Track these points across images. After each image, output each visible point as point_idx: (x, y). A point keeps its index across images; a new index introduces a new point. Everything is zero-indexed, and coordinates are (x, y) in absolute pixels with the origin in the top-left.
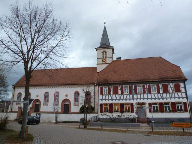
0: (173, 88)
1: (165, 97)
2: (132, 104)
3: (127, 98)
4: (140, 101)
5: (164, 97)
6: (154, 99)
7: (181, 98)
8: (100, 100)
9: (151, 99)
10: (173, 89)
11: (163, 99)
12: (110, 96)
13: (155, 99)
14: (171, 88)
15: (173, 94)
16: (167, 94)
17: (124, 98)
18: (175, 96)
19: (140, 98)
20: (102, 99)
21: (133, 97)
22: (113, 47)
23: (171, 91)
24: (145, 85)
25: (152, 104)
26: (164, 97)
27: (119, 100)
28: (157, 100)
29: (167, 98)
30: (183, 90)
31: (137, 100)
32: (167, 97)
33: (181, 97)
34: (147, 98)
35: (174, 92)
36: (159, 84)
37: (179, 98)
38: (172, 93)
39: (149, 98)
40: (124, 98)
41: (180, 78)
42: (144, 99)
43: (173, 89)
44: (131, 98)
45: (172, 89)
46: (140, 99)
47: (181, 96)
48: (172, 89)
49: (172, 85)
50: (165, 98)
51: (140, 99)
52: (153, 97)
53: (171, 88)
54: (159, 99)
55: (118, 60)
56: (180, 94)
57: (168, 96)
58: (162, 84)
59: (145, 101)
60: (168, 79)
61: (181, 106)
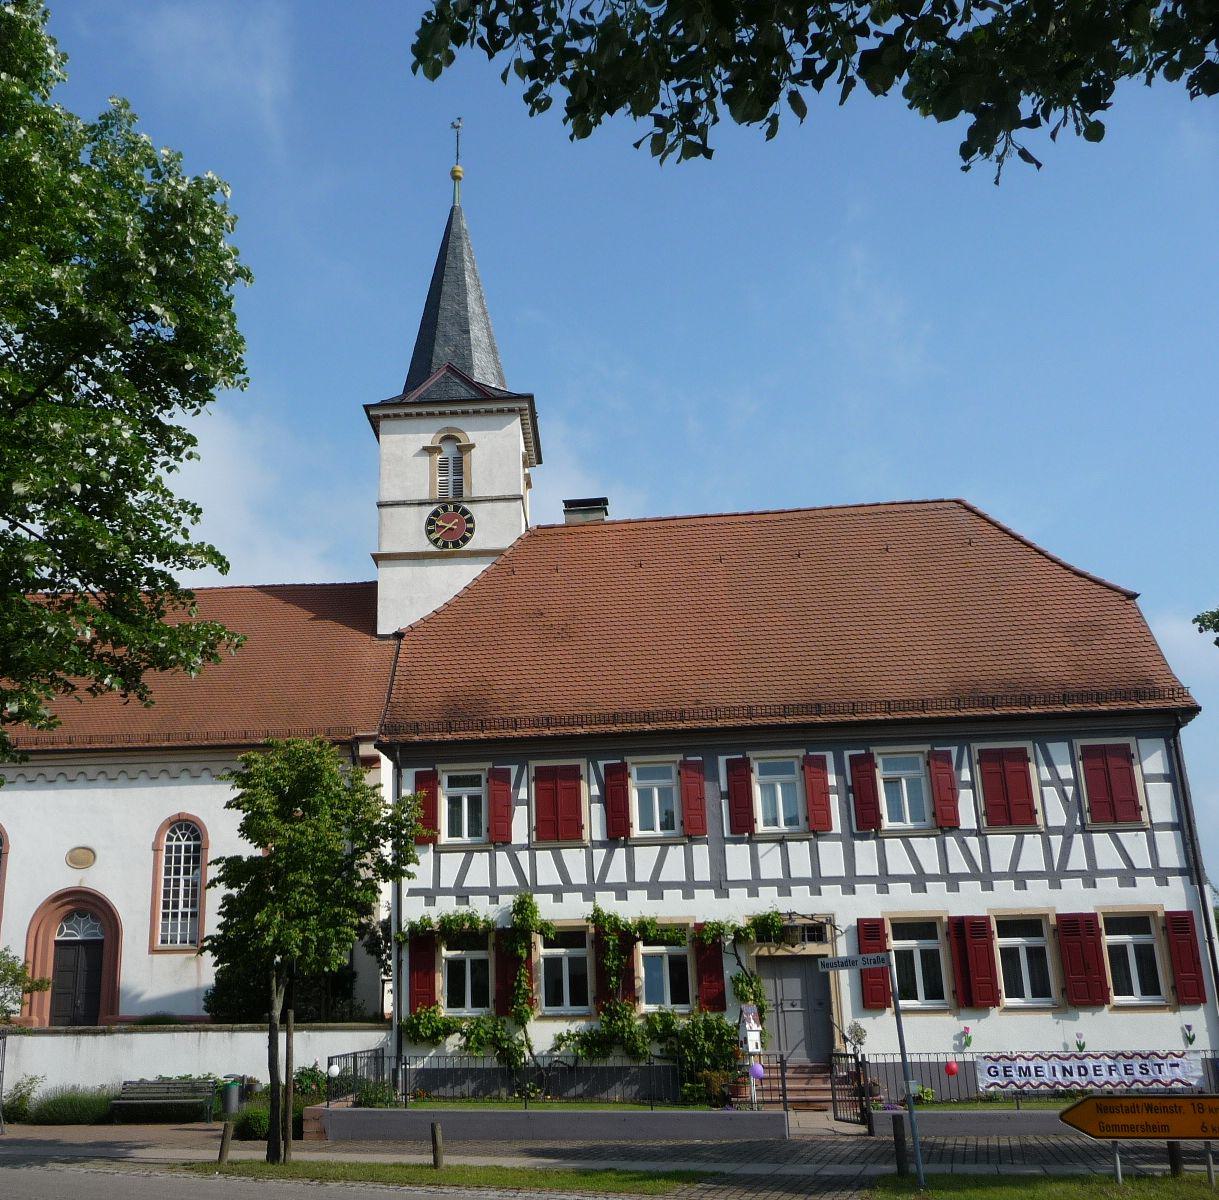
4: (784, 905)
5: (1000, 862)
11: (988, 886)
15: (1078, 839)
17: (639, 878)
19: (840, 871)
21: (719, 863)
22: (530, 398)
23: (1053, 809)
24: (830, 756)
25: (888, 929)
29: (1020, 879)
30: (1158, 802)
34: (683, 878)
36: (954, 750)
39: (801, 882)
40: (639, 878)
41: (1139, 695)
44: (703, 872)
46: (785, 885)
47: (1142, 860)
50: (1001, 876)
51: (785, 885)
54: (953, 881)
55: (579, 518)
56: (1135, 843)
57: (1033, 855)
58: (976, 747)
60: (1027, 701)
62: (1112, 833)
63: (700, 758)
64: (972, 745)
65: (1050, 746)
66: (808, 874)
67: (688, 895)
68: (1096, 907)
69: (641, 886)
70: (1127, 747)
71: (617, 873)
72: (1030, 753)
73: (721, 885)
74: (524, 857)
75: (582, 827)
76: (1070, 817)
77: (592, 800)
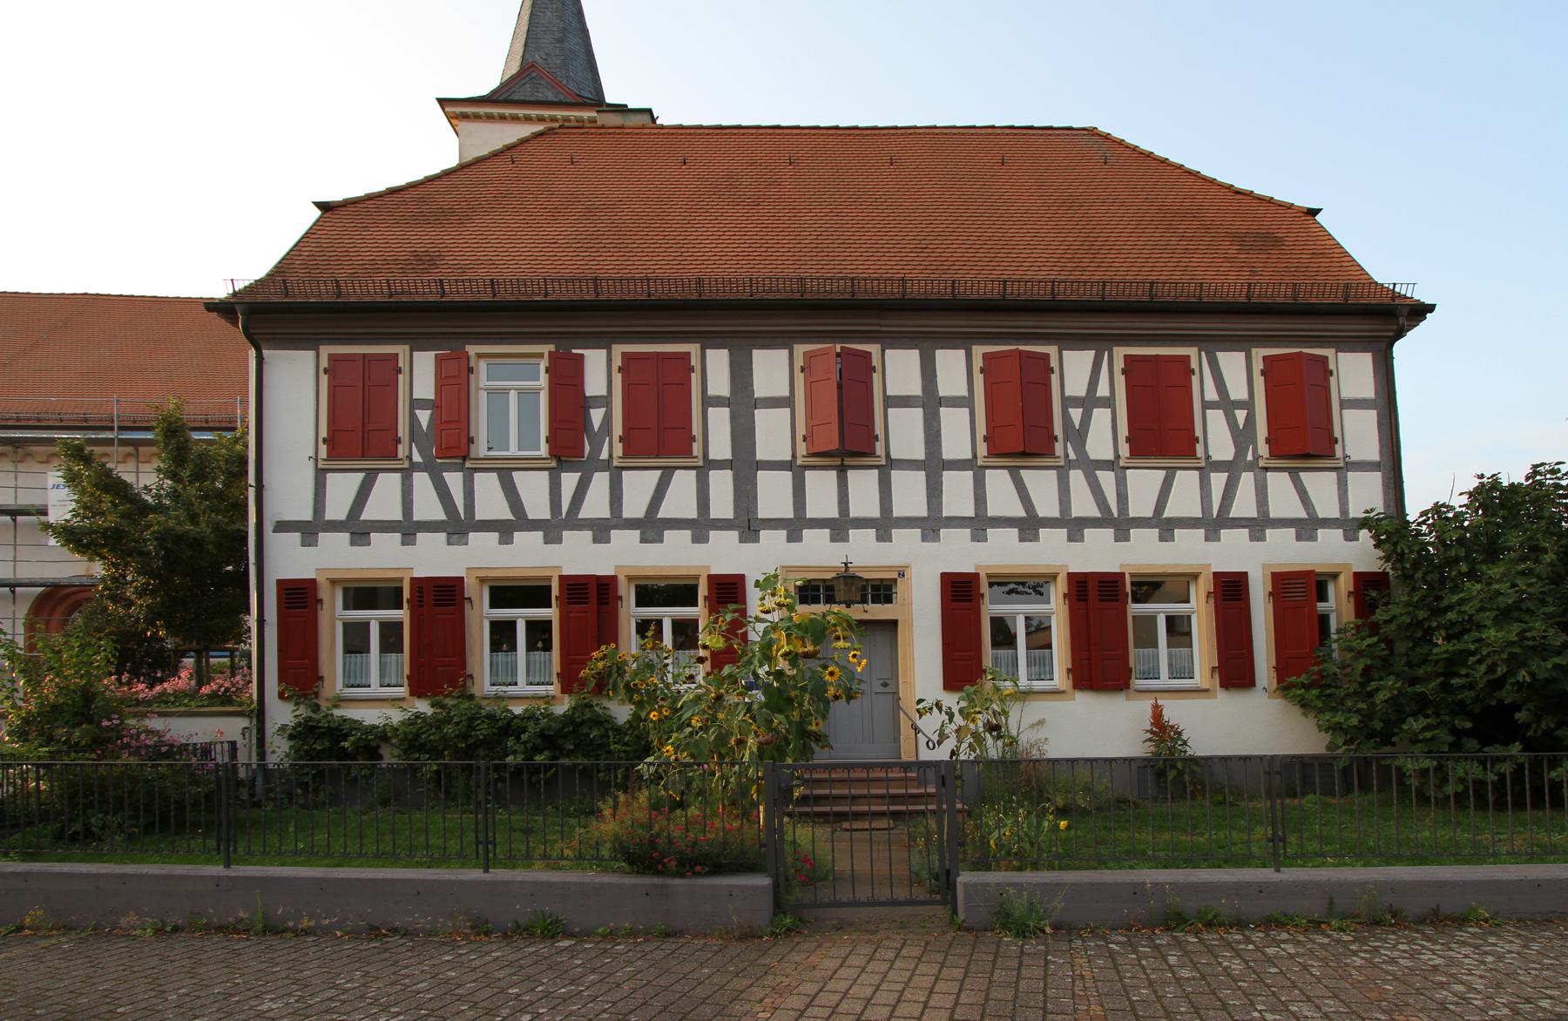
0: (1248, 405)
1: (1148, 512)
2: (1231, 589)
3: (369, 514)
5: (1142, 505)
6: (1338, 533)
7: (1050, 523)
8: (282, 527)
9: (980, 524)
10: (608, 419)
11: (1122, 536)
12: (1077, 478)
13: (1029, 526)
14: (1227, 404)
15: (1247, 480)
16: (1170, 473)
17: (627, 513)
18: (980, 498)
20: (788, 512)
23: (1218, 439)
24: (718, 364)
25: (628, 594)
26: (1142, 505)
27: (552, 530)
28: (1053, 538)
31: (795, 537)
32: (1168, 513)
33: (1054, 512)
34: (790, 515)
35: (1263, 449)
37: (1029, 526)
38: (1232, 469)
39: (956, 522)
40: (627, 513)
42: (885, 525)
43: (1250, 419)
45: (1241, 415)
46: (840, 527)
47: (1047, 506)
48: (1241, 415)
49: (953, 369)
50: (1142, 523)
52: (490, 501)
53: (1227, 404)
54: (1075, 528)
56: (1321, 485)
57: (1185, 497)
58: (1120, 352)
59: (905, 548)
61: (693, 623)
62: (1294, 473)
63: (574, 351)
64: (1115, 349)
65: (1220, 355)
66: (875, 512)
67: (700, 538)
68: (977, 567)
69: (631, 524)
70: (1324, 360)
71: (596, 505)
72: (1194, 364)
73: (748, 525)
74: (1107, 479)
75: (986, 439)
76: (1240, 450)
77: (606, 401)
